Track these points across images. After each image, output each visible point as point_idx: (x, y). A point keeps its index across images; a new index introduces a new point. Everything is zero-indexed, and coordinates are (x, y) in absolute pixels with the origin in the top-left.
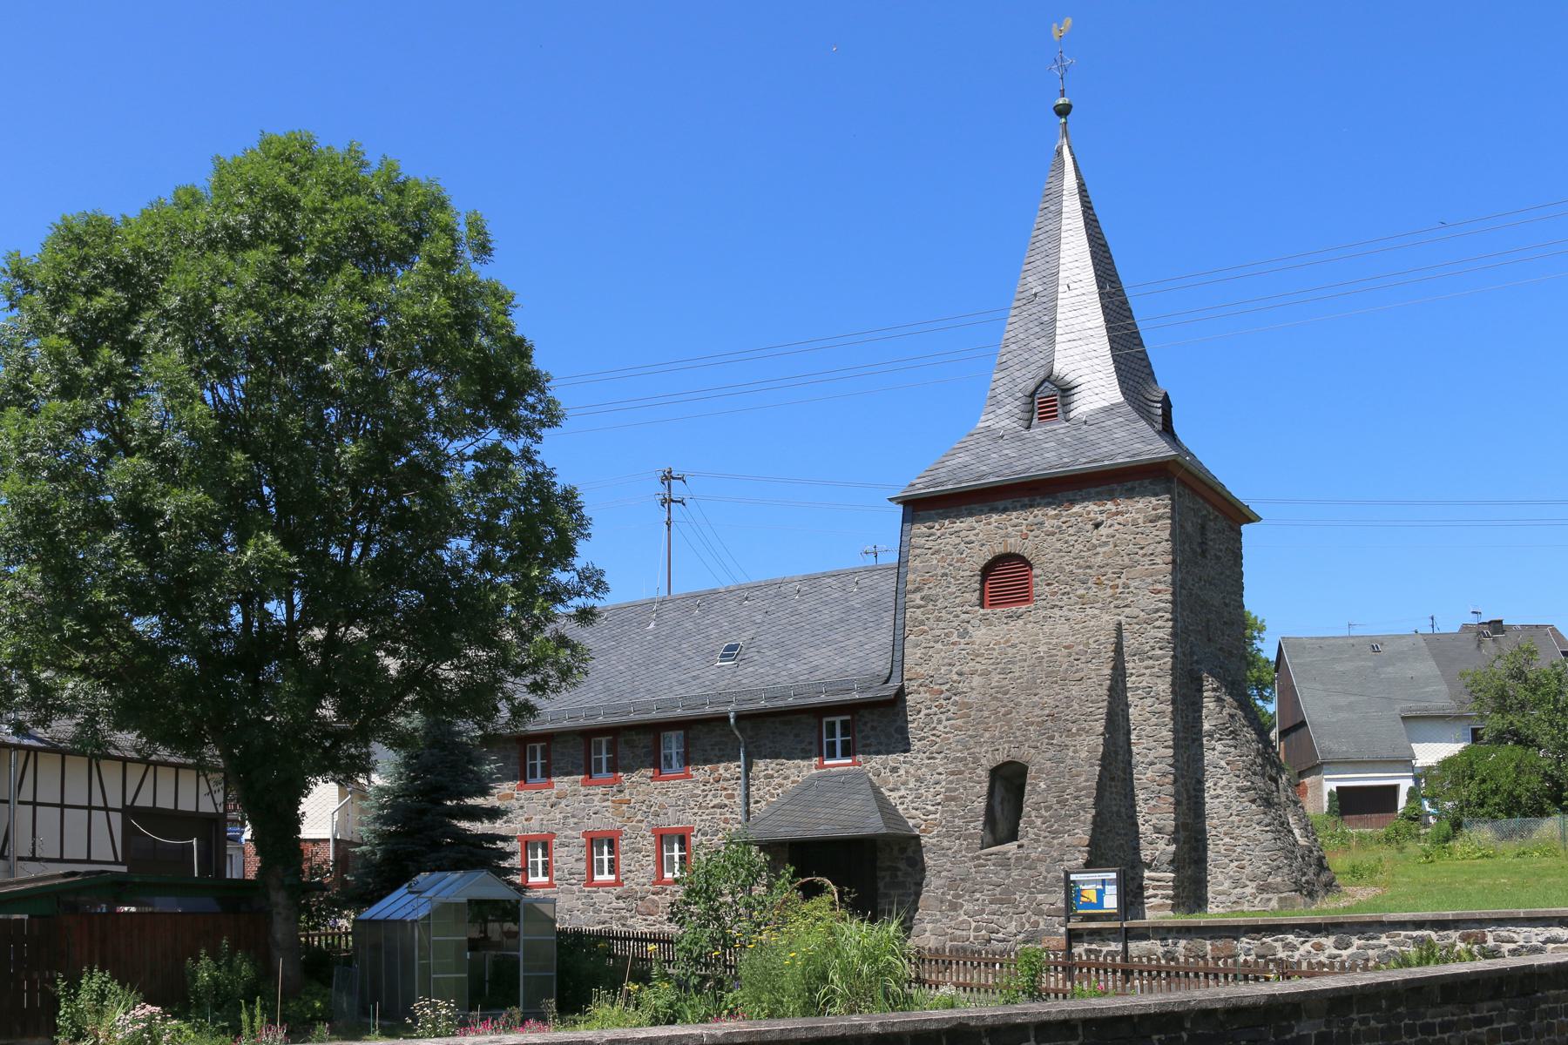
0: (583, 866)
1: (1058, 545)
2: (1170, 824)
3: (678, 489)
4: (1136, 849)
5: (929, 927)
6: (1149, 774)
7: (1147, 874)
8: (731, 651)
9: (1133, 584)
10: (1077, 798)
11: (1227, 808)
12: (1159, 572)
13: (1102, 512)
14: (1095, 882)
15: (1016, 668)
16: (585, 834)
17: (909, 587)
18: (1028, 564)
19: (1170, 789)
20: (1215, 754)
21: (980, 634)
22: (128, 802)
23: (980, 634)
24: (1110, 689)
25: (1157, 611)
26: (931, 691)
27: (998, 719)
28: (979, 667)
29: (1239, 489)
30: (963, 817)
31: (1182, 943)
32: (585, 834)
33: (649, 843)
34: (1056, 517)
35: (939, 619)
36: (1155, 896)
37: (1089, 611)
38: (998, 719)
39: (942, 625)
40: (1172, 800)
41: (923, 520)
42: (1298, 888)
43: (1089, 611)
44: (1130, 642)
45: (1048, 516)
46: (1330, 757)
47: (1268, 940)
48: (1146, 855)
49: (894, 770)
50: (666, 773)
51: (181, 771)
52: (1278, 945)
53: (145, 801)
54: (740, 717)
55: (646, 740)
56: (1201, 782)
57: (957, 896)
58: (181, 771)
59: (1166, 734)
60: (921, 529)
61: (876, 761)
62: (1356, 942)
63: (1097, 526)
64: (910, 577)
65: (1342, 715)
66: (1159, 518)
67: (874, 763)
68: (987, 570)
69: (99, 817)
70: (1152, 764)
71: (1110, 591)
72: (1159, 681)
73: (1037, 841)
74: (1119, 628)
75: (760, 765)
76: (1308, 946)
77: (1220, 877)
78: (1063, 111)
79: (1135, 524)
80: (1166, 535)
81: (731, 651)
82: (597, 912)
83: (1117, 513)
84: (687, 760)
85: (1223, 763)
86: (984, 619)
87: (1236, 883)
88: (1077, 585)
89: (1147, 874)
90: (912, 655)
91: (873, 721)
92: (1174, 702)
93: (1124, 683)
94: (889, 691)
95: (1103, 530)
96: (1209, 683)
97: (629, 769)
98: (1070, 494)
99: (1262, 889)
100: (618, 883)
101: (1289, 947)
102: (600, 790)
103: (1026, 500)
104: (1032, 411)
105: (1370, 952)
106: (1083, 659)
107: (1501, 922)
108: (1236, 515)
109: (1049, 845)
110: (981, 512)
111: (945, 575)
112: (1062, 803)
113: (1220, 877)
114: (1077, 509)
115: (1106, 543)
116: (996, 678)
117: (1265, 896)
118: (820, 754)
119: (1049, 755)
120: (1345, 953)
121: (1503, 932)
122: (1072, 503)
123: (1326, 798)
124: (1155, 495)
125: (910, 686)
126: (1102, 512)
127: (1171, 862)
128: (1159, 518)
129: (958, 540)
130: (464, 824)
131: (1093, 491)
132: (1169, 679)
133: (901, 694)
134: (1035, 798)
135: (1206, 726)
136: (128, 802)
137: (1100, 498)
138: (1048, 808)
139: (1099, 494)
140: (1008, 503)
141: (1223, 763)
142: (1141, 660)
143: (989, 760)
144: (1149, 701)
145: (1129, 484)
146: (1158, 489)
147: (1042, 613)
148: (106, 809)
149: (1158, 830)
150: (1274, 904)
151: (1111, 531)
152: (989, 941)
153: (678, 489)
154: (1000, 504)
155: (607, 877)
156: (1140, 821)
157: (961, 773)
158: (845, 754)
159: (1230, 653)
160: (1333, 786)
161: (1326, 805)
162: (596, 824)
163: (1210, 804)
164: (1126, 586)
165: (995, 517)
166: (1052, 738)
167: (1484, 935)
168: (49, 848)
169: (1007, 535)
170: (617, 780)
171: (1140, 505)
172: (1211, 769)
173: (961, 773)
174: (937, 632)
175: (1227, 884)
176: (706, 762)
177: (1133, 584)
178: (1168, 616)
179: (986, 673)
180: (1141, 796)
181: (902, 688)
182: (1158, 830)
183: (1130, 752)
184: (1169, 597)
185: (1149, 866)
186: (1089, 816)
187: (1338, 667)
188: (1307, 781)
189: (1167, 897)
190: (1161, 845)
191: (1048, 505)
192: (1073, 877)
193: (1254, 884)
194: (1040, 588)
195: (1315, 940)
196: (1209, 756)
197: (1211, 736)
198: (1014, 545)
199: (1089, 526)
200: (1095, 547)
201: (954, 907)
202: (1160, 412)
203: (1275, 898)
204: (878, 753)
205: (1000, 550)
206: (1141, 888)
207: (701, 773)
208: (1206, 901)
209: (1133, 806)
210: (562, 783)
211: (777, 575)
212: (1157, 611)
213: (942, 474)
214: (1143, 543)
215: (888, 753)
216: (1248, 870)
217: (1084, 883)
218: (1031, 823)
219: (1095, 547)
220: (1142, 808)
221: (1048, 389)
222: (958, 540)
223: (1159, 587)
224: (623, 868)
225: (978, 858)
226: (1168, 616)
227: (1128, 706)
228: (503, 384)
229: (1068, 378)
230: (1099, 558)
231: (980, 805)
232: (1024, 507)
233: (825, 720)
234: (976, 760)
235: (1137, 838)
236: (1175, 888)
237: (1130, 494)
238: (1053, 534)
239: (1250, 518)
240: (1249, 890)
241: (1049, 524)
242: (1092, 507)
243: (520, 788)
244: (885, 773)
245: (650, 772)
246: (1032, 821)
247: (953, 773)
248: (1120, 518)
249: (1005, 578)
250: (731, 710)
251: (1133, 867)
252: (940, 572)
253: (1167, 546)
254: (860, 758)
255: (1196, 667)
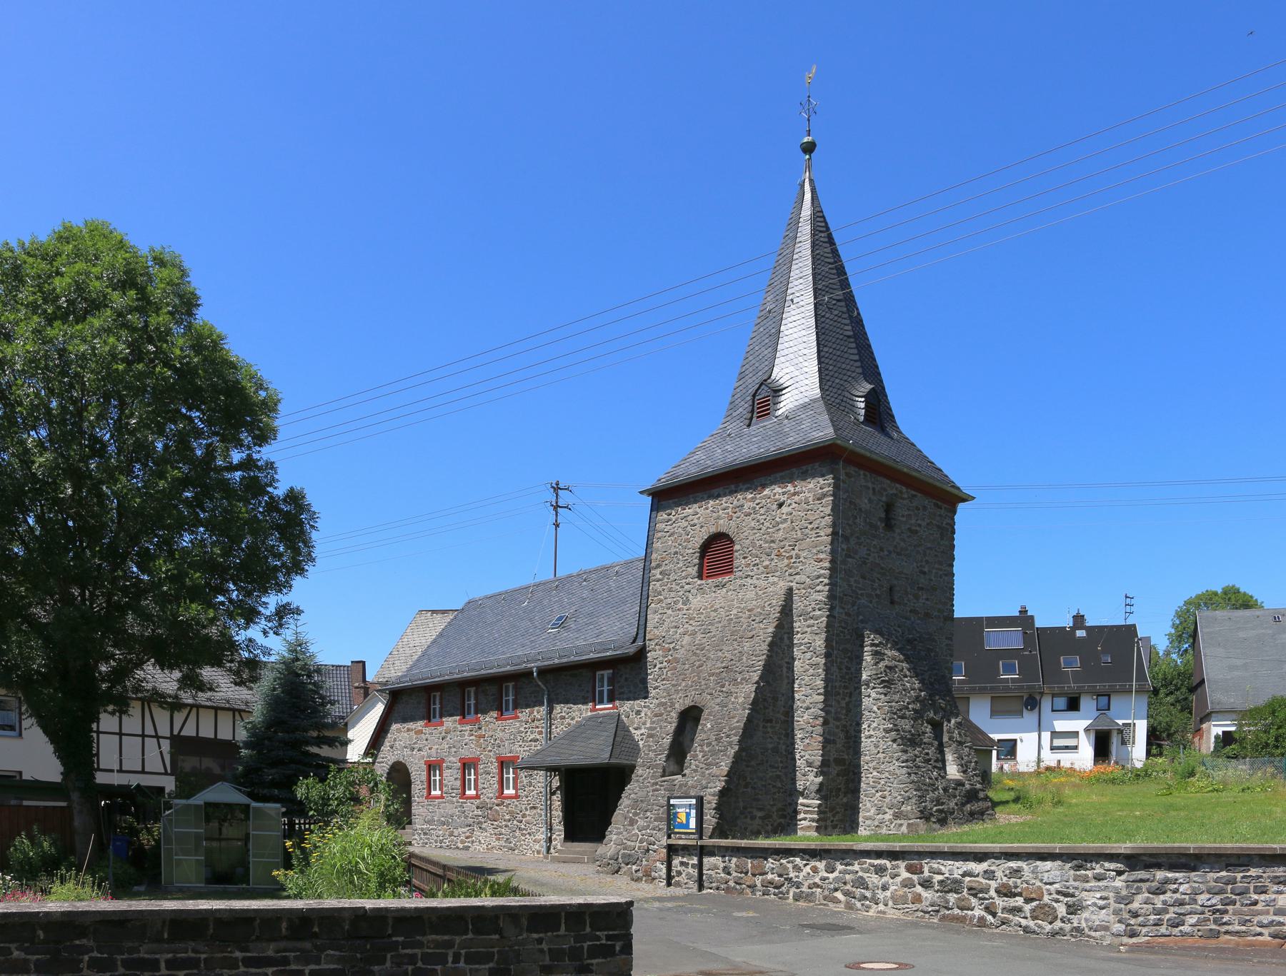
0: (458, 783)
1: (753, 524)
2: (818, 759)
3: (565, 498)
4: (794, 780)
5: (614, 837)
6: (806, 717)
7: (801, 800)
8: (562, 623)
9: (803, 554)
10: (728, 736)
11: (876, 746)
12: (821, 543)
13: (784, 494)
14: (684, 806)
15: (713, 629)
16: (426, 762)
17: (653, 564)
18: (732, 542)
19: (819, 729)
20: (872, 701)
21: (696, 601)
22: (175, 733)
23: (696, 601)
24: (771, 645)
25: (819, 577)
26: (663, 649)
27: (693, 671)
28: (691, 628)
29: (958, 474)
30: (655, 751)
31: (734, 860)
32: (426, 762)
33: (494, 768)
34: (753, 499)
35: (670, 590)
36: (805, 819)
37: (771, 579)
38: (693, 671)
39: (672, 594)
40: (821, 739)
41: (664, 509)
42: (925, 816)
43: (771, 579)
44: (798, 605)
45: (746, 499)
46: (1218, 708)
47: (783, 861)
48: (800, 785)
49: (638, 713)
50: (506, 715)
51: (201, 710)
52: (790, 866)
53: (189, 731)
54: (543, 672)
55: (493, 689)
56: (859, 724)
57: (636, 814)
58: (201, 710)
59: (820, 683)
60: (663, 516)
61: (628, 704)
62: (840, 867)
63: (780, 505)
64: (654, 556)
65: (1236, 673)
66: (824, 495)
67: (626, 707)
68: (705, 548)
69: (151, 742)
70: (808, 708)
71: (786, 561)
72: (817, 638)
73: (695, 771)
74: (790, 593)
75: (558, 708)
76: (808, 869)
77: (868, 805)
78: (809, 148)
79: (807, 503)
80: (828, 510)
81: (562, 623)
82: (466, 817)
83: (794, 494)
84: (516, 706)
85: (875, 708)
86: (700, 589)
87: (880, 810)
88: (764, 557)
89: (801, 800)
90: (653, 619)
91: (624, 672)
92: (827, 655)
93: (791, 639)
94: (632, 650)
95: (785, 509)
96: (870, 638)
97: (485, 712)
98: (763, 480)
99: (897, 816)
100: (477, 797)
101: (797, 869)
102: (468, 727)
103: (733, 487)
104: (752, 412)
105: (848, 877)
106: (758, 619)
107: (934, 855)
108: (947, 498)
109: (703, 775)
110: (703, 499)
111: (676, 553)
112: (718, 740)
113: (868, 805)
114: (767, 492)
115: (785, 520)
116: (699, 636)
117: (899, 822)
118: (594, 701)
119: (718, 700)
120: (831, 876)
121: (935, 864)
122: (764, 486)
123: (1213, 740)
124: (823, 476)
125: (651, 645)
126: (784, 494)
127: (818, 791)
128: (824, 495)
129: (686, 524)
130: (314, 750)
131: (778, 475)
132: (824, 636)
133: (641, 654)
134: (703, 736)
135: (864, 677)
136: (175, 733)
137: (782, 481)
138: (709, 744)
139: (782, 478)
140: (720, 490)
141: (875, 708)
142: (806, 620)
143: (679, 707)
144: (808, 655)
145: (804, 468)
146: (824, 470)
147: (739, 582)
148: (157, 737)
149: (810, 764)
150: (904, 829)
151: (789, 509)
152: (648, 850)
153: (565, 498)
154: (715, 492)
155: (511, 792)
156: (797, 756)
157: (661, 715)
158: (611, 700)
159: (927, 615)
160: (1219, 731)
161: (1212, 746)
162: (466, 753)
163: (866, 744)
164: (798, 557)
165: (711, 502)
166: (723, 686)
167: (922, 867)
168: (132, 763)
169: (718, 518)
170: (478, 720)
171: (811, 486)
172: (866, 713)
173: (661, 715)
174: (669, 601)
175: (873, 810)
176: (527, 706)
177: (803, 554)
178: (826, 581)
179: (694, 633)
180: (799, 735)
181: (644, 647)
182: (810, 764)
183: (793, 698)
184: (827, 565)
185: (802, 794)
186: (731, 752)
187: (1242, 635)
188: (1204, 726)
189: (812, 820)
190: (811, 777)
191: (747, 490)
192: (672, 802)
193: (891, 812)
194: (739, 561)
195: (813, 863)
196: (866, 702)
197: (868, 685)
198: (723, 526)
199: (775, 507)
200: (778, 524)
201: (632, 822)
202: (863, 405)
203: (905, 823)
204: (628, 699)
205: (713, 530)
206: (796, 812)
207: (524, 714)
208: (858, 824)
209: (793, 744)
210: (449, 722)
211: (607, 562)
212: (819, 577)
213: (680, 471)
214: (812, 518)
215: (635, 699)
216: (887, 800)
217: (680, 806)
218: (695, 757)
219: (778, 524)
220: (799, 745)
221: (764, 392)
222: (686, 524)
223: (822, 556)
224: (480, 786)
225: (656, 784)
226: (826, 581)
227: (794, 660)
228: (240, 409)
229: (781, 381)
230: (781, 533)
231: (667, 741)
232: (731, 493)
233: (598, 673)
234: (673, 704)
235: (795, 771)
236: (819, 813)
237: (804, 476)
238: (749, 514)
239: (965, 499)
240: (888, 817)
241: (748, 506)
242: (778, 489)
243: (426, 726)
244: (633, 715)
245: (494, 714)
246: (696, 758)
247: (656, 715)
248: (796, 498)
249: (716, 554)
250: (533, 666)
251: (791, 795)
252: (673, 550)
253: (829, 520)
254: (617, 703)
255: (861, 626)
